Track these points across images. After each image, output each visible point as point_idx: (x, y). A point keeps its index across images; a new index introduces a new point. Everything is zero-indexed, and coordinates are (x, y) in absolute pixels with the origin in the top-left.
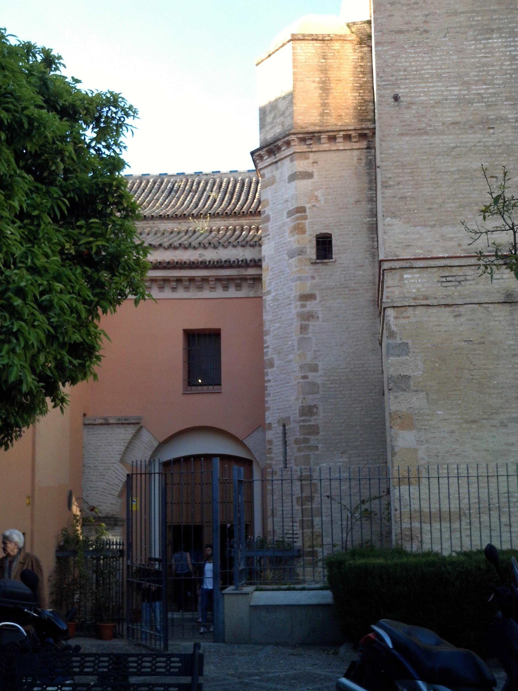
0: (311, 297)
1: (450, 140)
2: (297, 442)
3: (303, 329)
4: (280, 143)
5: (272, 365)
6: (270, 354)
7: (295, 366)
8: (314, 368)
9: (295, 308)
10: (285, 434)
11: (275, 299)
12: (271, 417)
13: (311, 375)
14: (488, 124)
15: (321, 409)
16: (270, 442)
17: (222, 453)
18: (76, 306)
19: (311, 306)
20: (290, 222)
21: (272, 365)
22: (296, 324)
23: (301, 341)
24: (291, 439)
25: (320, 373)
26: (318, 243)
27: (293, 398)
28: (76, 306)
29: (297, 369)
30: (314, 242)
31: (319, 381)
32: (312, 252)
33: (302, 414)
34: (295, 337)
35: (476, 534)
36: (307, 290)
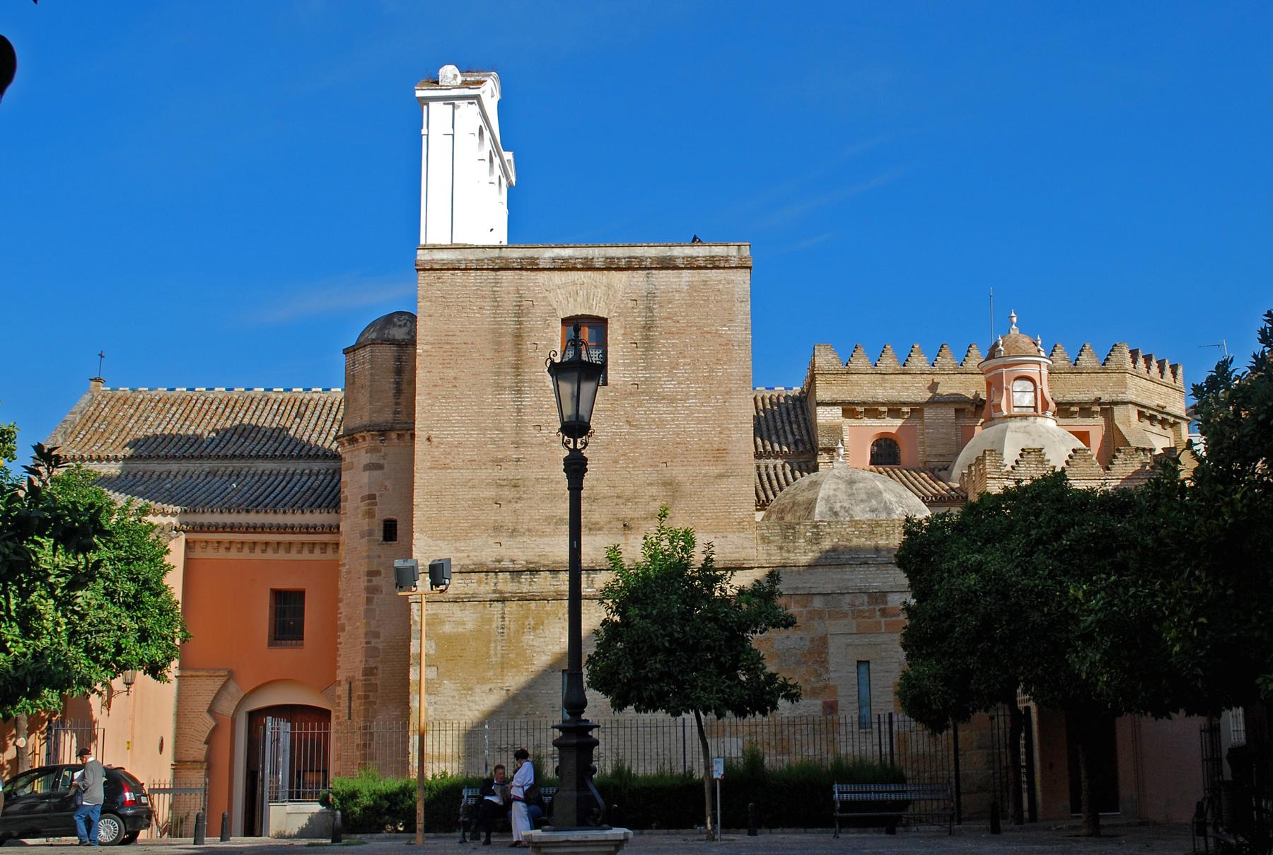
0: (378, 573)
1: (467, 474)
2: (359, 698)
3: (369, 601)
4: (357, 436)
5: (343, 630)
6: (343, 620)
7: (362, 631)
8: (376, 635)
9: (363, 583)
10: (350, 690)
11: (349, 572)
12: (341, 675)
13: (374, 641)
14: (498, 462)
15: (380, 671)
16: (339, 697)
17: (609, 362)
18: (169, 568)
19: (376, 581)
20: (363, 507)
21: (343, 630)
22: (364, 595)
23: (367, 611)
24: (355, 695)
25: (382, 639)
26: (385, 526)
27: (357, 660)
28: (169, 568)
29: (362, 635)
30: (382, 526)
31: (380, 646)
32: (379, 535)
33: (365, 674)
34: (362, 608)
35: (315, 435)
36: (375, 568)
